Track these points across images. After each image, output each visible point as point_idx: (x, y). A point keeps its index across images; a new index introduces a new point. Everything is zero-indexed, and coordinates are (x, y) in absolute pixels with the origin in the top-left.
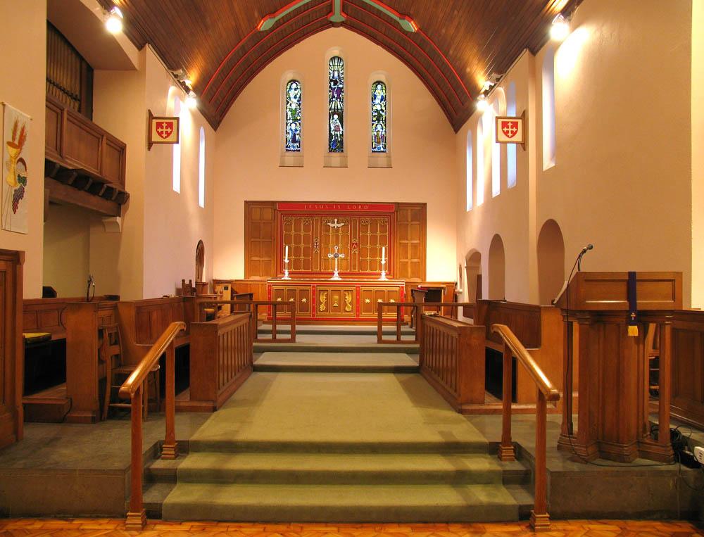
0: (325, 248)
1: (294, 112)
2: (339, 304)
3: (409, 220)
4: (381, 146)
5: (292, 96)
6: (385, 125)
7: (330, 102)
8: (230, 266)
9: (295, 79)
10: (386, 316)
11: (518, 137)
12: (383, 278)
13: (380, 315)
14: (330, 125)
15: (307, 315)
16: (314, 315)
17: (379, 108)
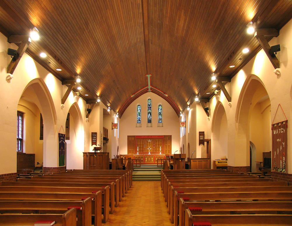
1: (139, 113)
5: (139, 109)
11: (185, 126)
12: (160, 154)
15: (143, 162)
17: (160, 111)
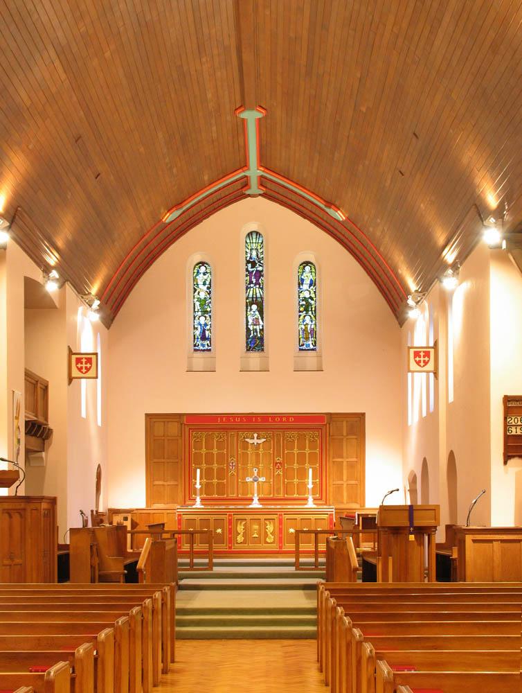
0: (243, 469)
1: (203, 303)
2: (259, 534)
3: (345, 434)
4: (310, 343)
5: (200, 283)
6: (315, 317)
7: (247, 288)
8: (130, 493)
9: (203, 260)
10: (303, 547)
11: (430, 366)
12: (310, 504)
13: (297, 547)
14: (247, 317)
15: (223, 547)
16: (230, 548)
